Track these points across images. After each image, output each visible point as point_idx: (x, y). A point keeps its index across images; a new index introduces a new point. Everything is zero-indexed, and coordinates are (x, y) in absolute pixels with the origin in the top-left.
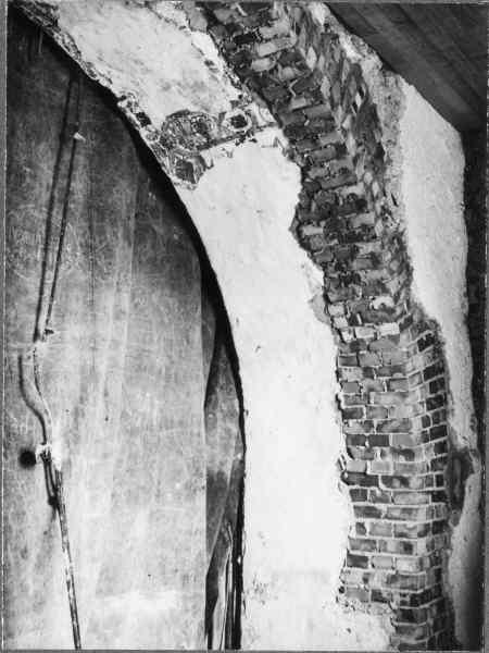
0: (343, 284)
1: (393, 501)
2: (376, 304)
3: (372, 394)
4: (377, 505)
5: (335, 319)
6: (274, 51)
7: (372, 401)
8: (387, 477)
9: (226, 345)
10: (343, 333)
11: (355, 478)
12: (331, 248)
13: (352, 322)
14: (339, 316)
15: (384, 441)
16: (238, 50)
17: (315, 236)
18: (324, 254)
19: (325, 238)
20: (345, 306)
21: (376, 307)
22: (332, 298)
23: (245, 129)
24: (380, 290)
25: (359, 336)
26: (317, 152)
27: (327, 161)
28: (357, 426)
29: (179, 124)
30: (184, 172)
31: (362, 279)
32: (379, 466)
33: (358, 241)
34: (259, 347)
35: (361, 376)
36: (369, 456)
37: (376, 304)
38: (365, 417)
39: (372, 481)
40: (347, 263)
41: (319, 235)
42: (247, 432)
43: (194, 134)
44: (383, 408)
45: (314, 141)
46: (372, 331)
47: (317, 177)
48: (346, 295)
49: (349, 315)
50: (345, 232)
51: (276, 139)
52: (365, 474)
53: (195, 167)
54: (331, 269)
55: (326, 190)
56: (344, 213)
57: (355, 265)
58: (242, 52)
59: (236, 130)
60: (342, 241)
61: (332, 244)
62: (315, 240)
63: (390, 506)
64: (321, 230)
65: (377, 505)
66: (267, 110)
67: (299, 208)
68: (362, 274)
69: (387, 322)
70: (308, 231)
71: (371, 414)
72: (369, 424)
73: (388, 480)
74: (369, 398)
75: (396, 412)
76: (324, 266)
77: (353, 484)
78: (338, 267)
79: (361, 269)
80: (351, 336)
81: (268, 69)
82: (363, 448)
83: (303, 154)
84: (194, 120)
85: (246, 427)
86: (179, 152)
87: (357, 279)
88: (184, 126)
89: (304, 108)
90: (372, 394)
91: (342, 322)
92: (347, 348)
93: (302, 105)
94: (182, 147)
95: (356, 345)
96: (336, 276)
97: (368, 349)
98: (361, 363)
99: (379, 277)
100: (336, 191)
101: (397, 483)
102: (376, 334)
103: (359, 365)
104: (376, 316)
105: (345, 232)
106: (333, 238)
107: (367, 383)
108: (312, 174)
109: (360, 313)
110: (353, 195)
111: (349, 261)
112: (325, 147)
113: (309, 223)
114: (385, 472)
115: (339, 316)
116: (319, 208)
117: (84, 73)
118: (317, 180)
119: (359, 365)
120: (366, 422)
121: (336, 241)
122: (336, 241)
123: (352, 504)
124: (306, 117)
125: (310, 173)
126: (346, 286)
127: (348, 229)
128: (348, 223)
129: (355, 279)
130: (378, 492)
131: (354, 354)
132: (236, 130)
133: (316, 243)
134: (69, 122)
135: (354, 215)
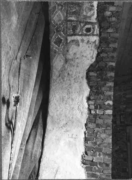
0: (97, 94)
1: (102, 172)
2: (106, 103)
3: (99, 133)
4: (96, 173)
5: (90, 106)
6: (114, 10)
7: (98, 136)
8: (101, 162)
10: (92, 111)
11: (88, 163)
12: (97, 82)
13: (96, 108)
14: (92, 105)
15: (100, 150)
16: (104, 6)
17: (93, 76)
19: (97, 77)
20: (95, 102)
21: (106, 104)
22: (92, 98)
23: (88, 33)
24: (109, 99)
25: (97, 113)
26: (107, 48)
28: (91, 144)
30: (58, 42)
32: (98, 159)
33: (108, 81)
35: (95, 127)
36: (94, 155)
37: (106, 103)
38: (94, 141)
39: (96, 164)
40: (101, 88)
41: (95, 76)
42: (45, 142)
44: (101, 138)
45: (108, 45)
46: (103, 112)
47: (103, 57)
48: (97, 98)
49: (95, 105)
50: (104, 77)
51: (96, 41)
52: (92, 161)
53: (62, 41)
54: (94, 88)
55: (104, 62)
57: (103, 89)
60: (102, 80)
62: (93, 77)
63: (101, 173)
64: (96, 75)
65: (96, 173)
66: (99, 29)
69: (109, 109)
70: (91, 74)
71: (97, 140)
72: (95, 143)
73: (100, 164)
74: (97, 134)
75: (106, 140)
77: (87, 165)
78: (97, 89)
79: (105, 90)
80: (95, 112)
81: (108, 15)
82: (92, 152)
83: (102, 47)
85: (30, 132)
86: (60, 34)
89: (111, 33)
90: (99, 133)
91: (92, 107)
92: (92, 116)
93: (111, 31)
94: (62, 33)
95: (95, 116)
96: (95, 91)
97: (99, 118)
98: (96, 122)
99: (110, 94)
101: (104, 165)
102: (104, 113)
103: (95, 123)
104: (105, 107)
105: (104, 77)
107: (96, 129)
108: (102, 55)
109: (100, 105)
110: (112, 65)
112: (110, 47)
113: (93, 71)
114: (100, 161)
115: (92, 105)
116: (99, 67)
117: (98, 16)
118: (102, 58)
119: (95, 123)
120: (95, 142)
121: (100, 79)
122: (100, 79)
123: (86, 172)
124: (110, 36)
128: (106, 74)
130: (97, 168)
131: (94, 119)
133: (93, 79)
134: (72, 33)
135: (109, 72)
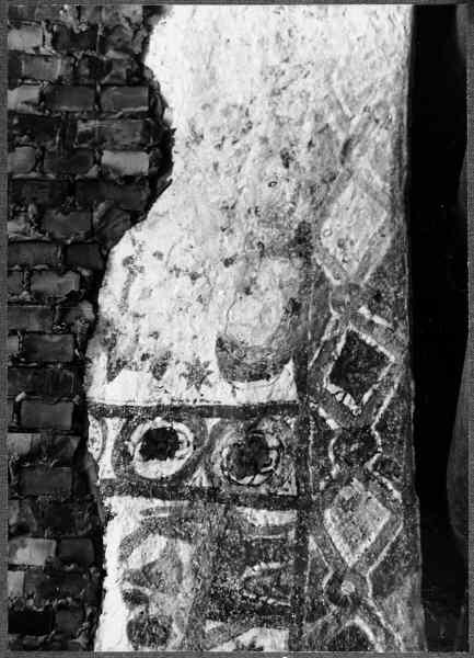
9: (94, 542)
18: (121, 104)
23: (159, 422)
26: (36, 327)
27: (22, 302)
29: (301, 479)
31: (49, 36)
34: (219, 146)
41: (114, 150)
43: (280, 448)
47: (61, 274)
50: (53, 145)
51: (111, 377)
56: (39, 183)
57: (59, 68)
58: (52, 595)
59: (177, 426)
60: (68, 123)
61: (93, 124)
64: (108, 158)
67: (136, 216)
68: (47, 49)
70: (140, 163)
76: (140, 77)
78: (99, 68)
79: (46, 58)
84: (258, 479)
87: (64, 38)
88: (291, 472)
94: (332, 424)
96: (111, 54)
100: (34, 235)
105: (53, 145)
106: (86, 136)
108: (71, 282)
111: (67, 81)
118: (68, 266)
121: (82, 127)
122: (82, 127)
125: (74, 287)
126: (93, 28)
127: (43, 149)
128: (39, 160)
129: (64, 40)
132: (177, 426)
133: (132, 133)
